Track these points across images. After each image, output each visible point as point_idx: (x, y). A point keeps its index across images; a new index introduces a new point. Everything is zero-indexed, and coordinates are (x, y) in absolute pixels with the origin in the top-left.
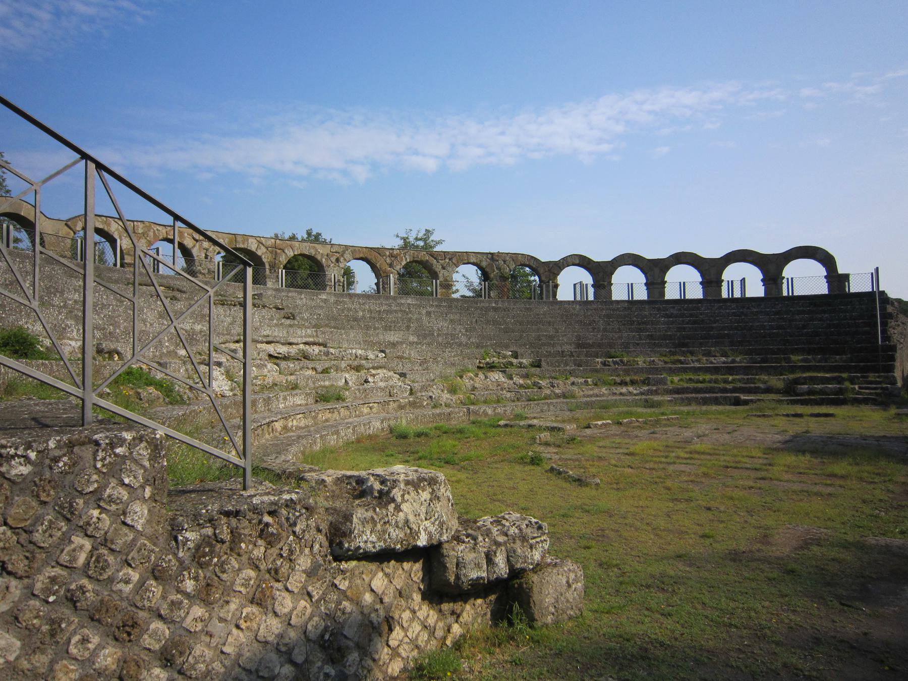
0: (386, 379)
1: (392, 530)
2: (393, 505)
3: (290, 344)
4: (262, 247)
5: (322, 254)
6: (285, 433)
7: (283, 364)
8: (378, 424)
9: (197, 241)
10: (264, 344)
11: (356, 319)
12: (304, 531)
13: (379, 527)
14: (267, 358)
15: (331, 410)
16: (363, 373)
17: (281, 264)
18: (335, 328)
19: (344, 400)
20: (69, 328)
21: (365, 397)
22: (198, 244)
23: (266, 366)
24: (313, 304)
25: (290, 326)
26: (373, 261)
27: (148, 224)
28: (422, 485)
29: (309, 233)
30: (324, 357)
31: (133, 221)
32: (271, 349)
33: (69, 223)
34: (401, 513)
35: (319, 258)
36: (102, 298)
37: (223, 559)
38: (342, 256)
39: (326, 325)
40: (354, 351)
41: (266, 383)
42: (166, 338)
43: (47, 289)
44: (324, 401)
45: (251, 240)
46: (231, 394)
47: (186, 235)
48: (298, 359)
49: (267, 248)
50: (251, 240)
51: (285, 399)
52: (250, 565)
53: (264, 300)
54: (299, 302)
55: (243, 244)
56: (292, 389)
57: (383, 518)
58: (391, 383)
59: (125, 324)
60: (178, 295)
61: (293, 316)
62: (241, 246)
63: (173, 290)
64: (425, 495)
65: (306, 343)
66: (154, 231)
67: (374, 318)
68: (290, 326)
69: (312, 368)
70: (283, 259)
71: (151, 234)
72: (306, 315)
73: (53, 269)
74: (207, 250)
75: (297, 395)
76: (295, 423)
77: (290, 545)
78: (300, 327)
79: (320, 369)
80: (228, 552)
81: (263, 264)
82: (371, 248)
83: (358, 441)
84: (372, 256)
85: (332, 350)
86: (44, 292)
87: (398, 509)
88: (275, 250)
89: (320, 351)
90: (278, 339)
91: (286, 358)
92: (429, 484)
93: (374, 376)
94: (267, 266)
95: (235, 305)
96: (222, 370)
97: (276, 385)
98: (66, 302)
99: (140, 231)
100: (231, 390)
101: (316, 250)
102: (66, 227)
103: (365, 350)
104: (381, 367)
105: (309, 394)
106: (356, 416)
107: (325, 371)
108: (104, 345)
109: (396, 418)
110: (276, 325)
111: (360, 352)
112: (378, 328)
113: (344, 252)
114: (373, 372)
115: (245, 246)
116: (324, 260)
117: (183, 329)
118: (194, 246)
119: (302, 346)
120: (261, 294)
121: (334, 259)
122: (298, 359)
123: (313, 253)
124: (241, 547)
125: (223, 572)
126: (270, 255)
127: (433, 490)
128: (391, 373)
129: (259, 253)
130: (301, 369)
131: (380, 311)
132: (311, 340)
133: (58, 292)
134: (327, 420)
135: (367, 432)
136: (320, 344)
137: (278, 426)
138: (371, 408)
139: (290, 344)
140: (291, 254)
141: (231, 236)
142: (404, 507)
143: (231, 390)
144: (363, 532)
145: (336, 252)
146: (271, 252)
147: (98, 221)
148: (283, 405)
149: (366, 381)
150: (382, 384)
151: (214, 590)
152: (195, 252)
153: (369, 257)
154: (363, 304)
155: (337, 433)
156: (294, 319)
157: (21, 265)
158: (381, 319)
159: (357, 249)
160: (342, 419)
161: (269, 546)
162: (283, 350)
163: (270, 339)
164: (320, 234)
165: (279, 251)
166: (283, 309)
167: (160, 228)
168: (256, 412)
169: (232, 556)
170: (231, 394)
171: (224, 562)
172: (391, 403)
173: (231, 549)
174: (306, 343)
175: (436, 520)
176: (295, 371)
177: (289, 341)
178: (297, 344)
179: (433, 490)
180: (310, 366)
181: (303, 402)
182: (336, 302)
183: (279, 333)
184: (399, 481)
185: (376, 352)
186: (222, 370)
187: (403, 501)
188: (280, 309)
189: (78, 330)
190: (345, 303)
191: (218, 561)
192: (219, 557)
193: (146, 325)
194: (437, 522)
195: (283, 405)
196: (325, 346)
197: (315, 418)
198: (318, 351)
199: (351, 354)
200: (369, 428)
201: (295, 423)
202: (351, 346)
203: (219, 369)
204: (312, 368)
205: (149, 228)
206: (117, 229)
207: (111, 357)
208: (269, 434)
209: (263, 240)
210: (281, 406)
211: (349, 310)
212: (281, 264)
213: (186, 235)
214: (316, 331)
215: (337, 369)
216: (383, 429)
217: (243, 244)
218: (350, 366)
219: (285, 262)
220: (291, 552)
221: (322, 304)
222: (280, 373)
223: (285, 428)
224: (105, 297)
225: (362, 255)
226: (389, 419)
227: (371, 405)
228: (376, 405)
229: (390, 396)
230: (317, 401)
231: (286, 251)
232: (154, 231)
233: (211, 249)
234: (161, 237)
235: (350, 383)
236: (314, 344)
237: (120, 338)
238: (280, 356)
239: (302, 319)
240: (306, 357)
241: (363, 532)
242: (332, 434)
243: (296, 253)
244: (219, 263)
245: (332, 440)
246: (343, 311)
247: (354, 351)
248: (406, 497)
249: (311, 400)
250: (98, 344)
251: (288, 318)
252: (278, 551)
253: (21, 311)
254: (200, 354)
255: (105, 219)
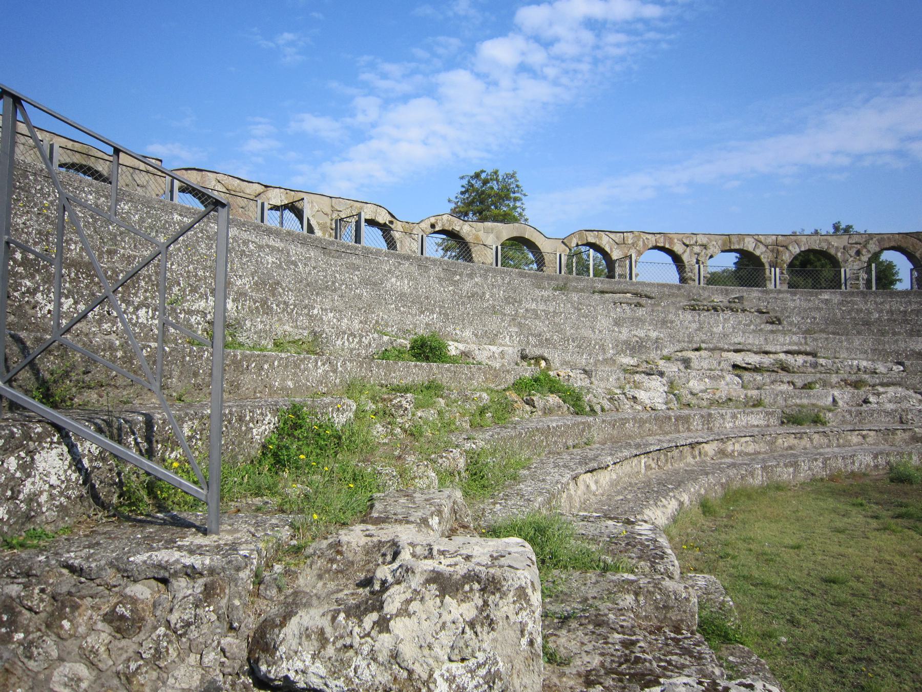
0: (898, 400)
1: (364, 664)
2: (374, 616)
3: (766, 353)
4: (761, 246)
5: (837, 248)
6: (721, 458)
7: (747, 376)
8: (868, 460)
9: (687, 246)
10: (732, 353)
11: (867, 323)
12: (188, 624)
13: (330, 651)
14: (730, 368)
15: (799, 436)
16: (862, 392)
17: (784, 263)
18: (833, 333)
19: (824, 424)
20: (502, 334)
21: (860, 421)
22: (688, 249)
23: (723, 377)
24: (811, 305)
25: (772, 332)
26: (911, 249)
27: (637, 234)
28: (467, 587)
29: (836, 228)
30: (810, 370)
31: (623, 233)
32: (738, 359)
33: (565, 241)
34: (385, 636)
35: (832, 252)
36: (559, 306)
37: (31, 637)
38: (865, 247)
39: (822, 331)
40: (855, 362)
41: (717, 397)
42: (610, 346)
43: (506, 299)
44: (793, 423)
45: (747, 239)
46: (664, 407)
47: (676, 241)
48: (773, 371)
49: (767, 246)
50: (747, 239)
51: (734, 416)
52: (81, 658)
53: (746, 303)
54: (791, 304)
55: (739, 244)
56: (754, 406)
57: (342, 637)
58: (905, 405)
59: (572, 331)
60: (643, 301)
61: (779, 320)
62: (737, 247)
63: (641, 296)
64: (468, 610)
65: (787, 352)
66: (644, 240)
67: (895, 321)
68: (772, 332)
69: (788, 382)
70: (787, 258)
71: (641, 243)
72: (795, 319)
73: (522, 281)
74: (698, 254)
75: (752, 413)
76: (737, 447)
77: (158, 642)
78: (784, 333)
79: (799, 383)
80: (43, 628)
81: (762, 265)
82: (907, 234)
83: (832, 478)
84: (908, 244)
85: (822, 361)
86: (502, 302)
87: (383, 625)
88: (777, 247)
89: (806, 362)
90: (749, 347)
91: (756, 370)
92: (483, 590)
93: (879, 394)
94: (767, 266)
95: (708, 310)
96: (664, 380)
97: (730, 400)
98: (517, 311)
99: (630, 241)
100: (666, 403)
101: (830, 243)
102: (563, 245)
103: (873, 361)
104: (893, 384)
105: (772, 414)
106: (838, 446)
107: (808, 386)
108: (527, 351)
109: (900, 454)
110: (754, 331)
111: (864, 363)
112: (899, 333)
113: (867, 242)
114: (881, 389)
115: (741, 247)
116: (839, 254)
117: (637, 336)
118: (685, 252)
119: (782, 356)
120: (742, 297)
121: (853, 252)
122: (773, 371)
123: (825, 246)
124: (62, 627)
125: (30, 657)
126: (771, 254)
127: (486, 603)
128: (911, 392)
129: (757, 253)
130: (772, 382)
131: (905, 312)
132: (795, 348)
133: (516, 302)
134: (791, 448)
135: (849, 469)
136: (807, 354)
137: (710, 449)
138: (864, 437)
139: (766, 353)
140: (796, 250)
141: (724, 237)
142: (397, 625)
143: (666, 403)
144: (296, 652)
145: (856, 243)
146: (772, 251)
147: (591, 236)
148: (731, 424)
149: (866, 401)
150: (890, 407)
151: (13, 680)
152: (685, 258)
153: (904, 245)
154: (882, 303)
155: (795, 465)
156: (780, 323)
157: (493, 280)
158: (906, 321)
159: (885, 237)
160: (815, 447)
161: (119, 636)
162: (753, 359)
163: (739, 347)
164: (850, 227)
165: (781, 249)
166: (768, 313)
167: (649, 236)
168: (689, 430)
169: (48, 636)
170: (664, 407)
171: (31, 643)
172: (899, 432)
173: (48, 626)
174: (787, 352)
175: (479, 666)
176: (764, 385)
177: (763, 349)
178: (775, 353)
179: (486, 603)
180: (785, 380)
181: (762, 422)
182: (841, 303)
183: (755, 341)
184: (413, 572)
185: (890, 365)
186: (664, 380)
187: (404, 612)
188: (764, 313)
189: (753, 345)
190: (854, 303)
191: (25, 638)
192: (27, 633)
193: (595, 332)
194: (483, 672)
195: (731, 424)
196: (814, 355)
197: (772, 443)
198: (801, 361)
199: (851, 366)
200: (853, 463)
201: (737, 447)
202: (853, 356)
203: (660, 379)
204: (788, 382)
205: (638, 238)
206: (608, 242)
207: (537, 363)
208: (694, 457)
209: (762, 238)
210: (729, 425)
211: (859, 311)
212: (784, 263)
213: (676, 241)
214: (805, 338)
215: (825, 384)
216: (876, 466)
217: (739, 244)
218: (845, 381)
219: (789, 261)
220: (158, 654)
221: (821, 305)
222: (742, 387)
223: (722, 453)
224: (562, 305)
225: (892, 244)
226: (888, 455)
227: (864, 433)
228: (872, 433)
229: (902, 422)
230: (783, 423)
231: (790, 248)
232: (644, 240)
233: (703, 253)
234: (650, 246)
235: (840, 403)
236: (799, 353)
237: (558, 345)
238: (749, 366)
239: (791, 324)
240: (785, 368)
241: (296, 652)
242: (786, 466)
243: (803, 249)
244: (497, 248)
245: (785, 474)
246: (849, 312)
247: (855, 362)
248: (415, 606)
249: (773, 421)
250: (522, 350)
251: (772, 323)
252: (135, 647)
253: (464, 319)
254: (647, 362)
255: (596, 233)
